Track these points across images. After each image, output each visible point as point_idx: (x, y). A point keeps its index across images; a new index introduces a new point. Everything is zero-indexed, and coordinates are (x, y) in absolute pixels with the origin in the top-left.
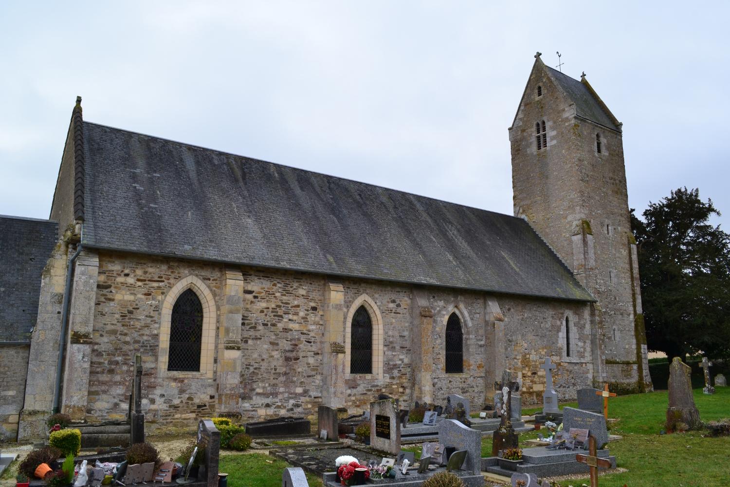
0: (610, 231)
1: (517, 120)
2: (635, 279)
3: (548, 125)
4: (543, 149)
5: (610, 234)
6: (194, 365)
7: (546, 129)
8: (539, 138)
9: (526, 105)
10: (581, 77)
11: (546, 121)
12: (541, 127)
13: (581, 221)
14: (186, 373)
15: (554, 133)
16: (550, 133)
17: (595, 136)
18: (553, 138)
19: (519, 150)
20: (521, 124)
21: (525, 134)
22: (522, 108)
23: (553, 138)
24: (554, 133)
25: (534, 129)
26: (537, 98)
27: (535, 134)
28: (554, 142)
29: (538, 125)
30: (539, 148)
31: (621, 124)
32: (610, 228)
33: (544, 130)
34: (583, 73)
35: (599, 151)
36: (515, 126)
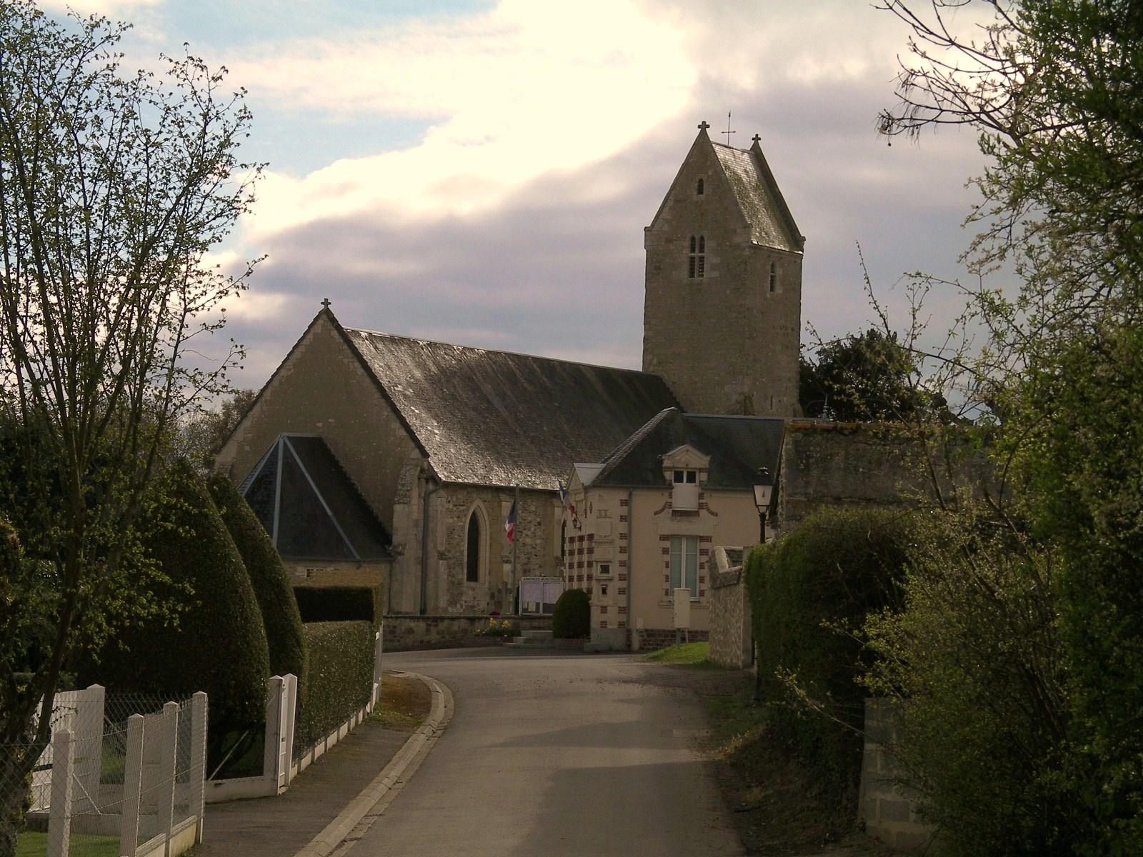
0: (774, 404)
1: (660, 220)
2: (451, 622)
3: (709, 244)
4: (697, 279)
5: (774, 409)
6: (365, 594)
7: (705, 250)
8: (692, 259)
9: (676, 201)
10: (753, 139)
11: (706, 238)
12: (697, 244)
13: (742, 397)
14: (374, 596)
15: (716, 260)
16: (711, 259)
17: (769, 268)
18: (714, 267)
19: (660, 269)
20: (666, 228)
21: (672, 247)
22: (670, 203)
23: (714, 267)
24: (716, 260)
25: (687, 243)
26: (696, 197)
27: (687, 252)
28: (715, 274)
29: (693, 239)
30: (692, 274)
31: (804, 239)
32: (774, 400)
33: (702, 249)
34: (757, 135)
35: (772, 289)
36: (656, 227)
